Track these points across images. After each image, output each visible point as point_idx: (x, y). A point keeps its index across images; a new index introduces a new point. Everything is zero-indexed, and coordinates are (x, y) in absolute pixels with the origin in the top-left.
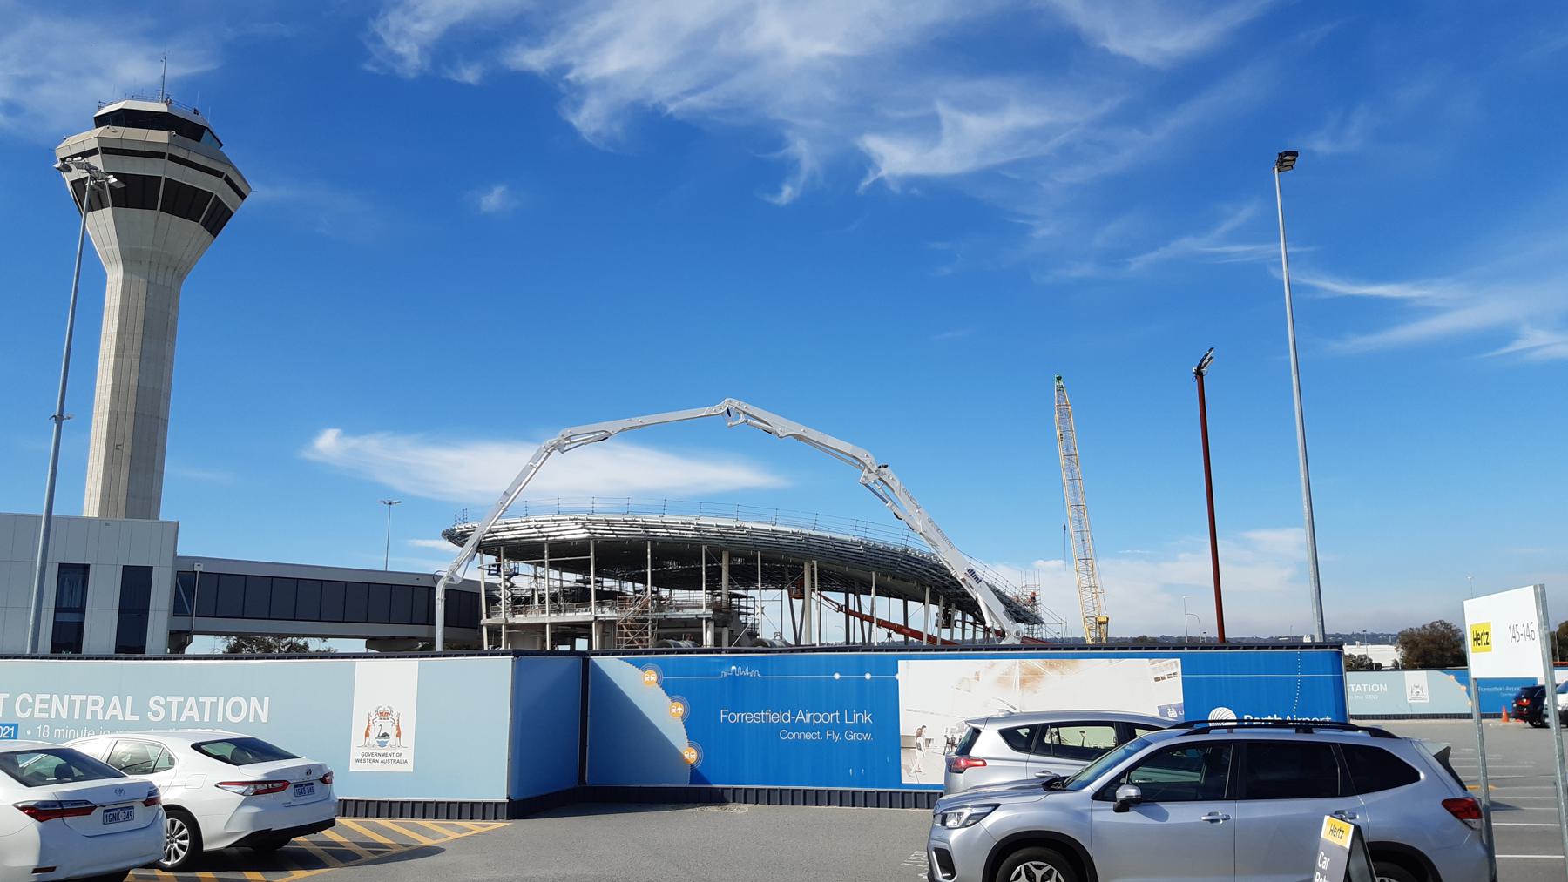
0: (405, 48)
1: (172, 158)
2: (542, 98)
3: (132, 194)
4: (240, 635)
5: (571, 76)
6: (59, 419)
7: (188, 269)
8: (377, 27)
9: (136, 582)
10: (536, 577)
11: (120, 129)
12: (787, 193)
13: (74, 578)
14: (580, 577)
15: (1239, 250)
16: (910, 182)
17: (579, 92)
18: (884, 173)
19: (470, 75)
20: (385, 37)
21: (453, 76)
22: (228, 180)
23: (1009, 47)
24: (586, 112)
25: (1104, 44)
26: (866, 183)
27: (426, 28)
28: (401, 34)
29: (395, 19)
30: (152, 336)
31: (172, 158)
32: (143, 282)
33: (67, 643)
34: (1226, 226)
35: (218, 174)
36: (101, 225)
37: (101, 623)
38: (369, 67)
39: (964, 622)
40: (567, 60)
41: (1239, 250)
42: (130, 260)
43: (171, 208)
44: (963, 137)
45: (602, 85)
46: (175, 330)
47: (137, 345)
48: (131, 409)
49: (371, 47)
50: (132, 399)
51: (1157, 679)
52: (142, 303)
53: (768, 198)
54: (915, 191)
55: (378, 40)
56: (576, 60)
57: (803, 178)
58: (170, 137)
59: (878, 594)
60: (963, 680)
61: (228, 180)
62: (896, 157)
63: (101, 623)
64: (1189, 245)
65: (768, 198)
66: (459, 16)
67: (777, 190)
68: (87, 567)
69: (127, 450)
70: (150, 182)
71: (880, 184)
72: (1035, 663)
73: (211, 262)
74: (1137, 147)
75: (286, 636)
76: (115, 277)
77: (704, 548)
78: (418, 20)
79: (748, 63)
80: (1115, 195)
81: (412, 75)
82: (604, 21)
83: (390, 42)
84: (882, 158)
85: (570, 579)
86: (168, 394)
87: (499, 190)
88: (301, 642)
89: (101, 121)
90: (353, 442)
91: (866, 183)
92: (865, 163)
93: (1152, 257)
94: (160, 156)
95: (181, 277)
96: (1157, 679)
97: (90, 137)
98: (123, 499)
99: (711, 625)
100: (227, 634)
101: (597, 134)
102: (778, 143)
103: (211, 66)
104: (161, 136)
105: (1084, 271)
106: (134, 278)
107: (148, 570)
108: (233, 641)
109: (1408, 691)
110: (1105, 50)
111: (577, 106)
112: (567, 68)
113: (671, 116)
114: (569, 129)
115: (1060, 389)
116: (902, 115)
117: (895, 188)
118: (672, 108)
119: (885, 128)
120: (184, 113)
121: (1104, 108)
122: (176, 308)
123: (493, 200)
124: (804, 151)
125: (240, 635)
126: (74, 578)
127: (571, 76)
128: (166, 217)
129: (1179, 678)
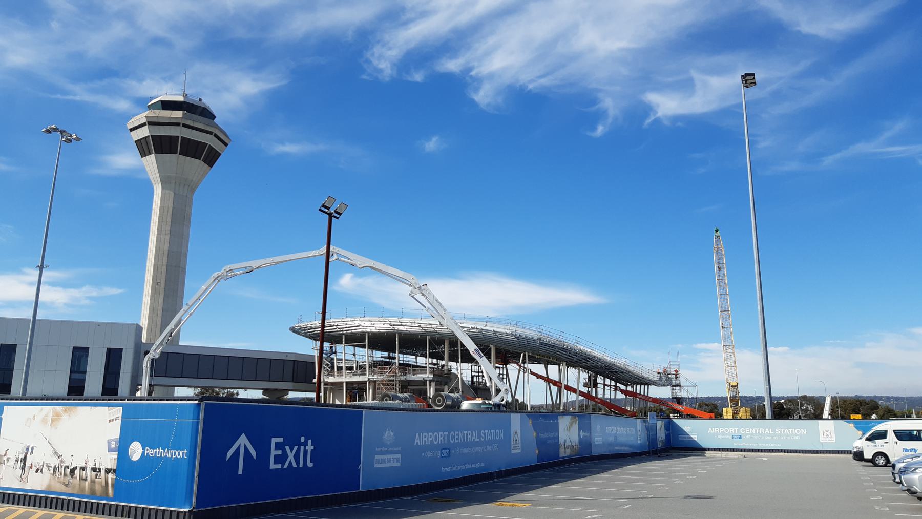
0: (384, 65)
1: (184, 125)
2: (455, 88)
3: (160, 145)
4: (202, 388)
5: (473, 73)
6: (41, 268)
7: (197, 185)
8: (368, 55)
9: (113, 357)
10: (354, 355)
11: (157, 111)
12: (600, 130)
13: (80, 355)
14: (386, 354)
15: (897, 150)
16: (676, 118)
17: (478, 81)
18: (660, 114)
19: (418, 77)
20: (372, 59)
21: (410, 79)
22: (216, 136)
23: (734, 34)
24: (482, 93)
25: (798, 28)
26: (648, 121)
27: (394, 53)
28: (381, 57)
29: (377, 50)
30: (178, 222)
31: (184, 125)
32: (172, 193)
33: (76, 390)
34: (887, 134)
35: (211, 133)
36: (151, 162)
37: (94, 382)
38: (364, 77)
39: (605, 385)
40: (471, 64)
41: (897, 150)
42: (165, 182)
43: (185, 153)
44: (712, 89)
45: (491, 76)
46: (190, 219)
47: (168, 228)
48: (165, 263)
49: (365, 66)
50: (165, 258)
51: (110, 421)
52: (171, 205)
53: (589, 133)
54: (680, 124)
55: (368, 61)
56: (476, 64)
57: (610, 120)
58: (184, 114)
59: (462, 362)
60: (29, 419)
61: (216, 136)
62: (667, 105)
63: (94, 382)
64: (863, 148)
65: (589, 133)
66: (412, 45)
67: (594, 129)
68: (87, 349)
69: (163, 285)
70: (173, 140)
71: (657, 121)
72: (59, 408)
73: (212, 182)
74: (821, 90)
75: (224, 389)
76: (158, 190)
77: (428, 338)
78: (390, 49)
79: (575, 57)
80: (814, 118)
81: (387, 79)
82: (491, 41)
83: (375, 62)
84: (658, 105)
85: (378, 355)
86: (186, 255)
87: (435, 139)
88: (235, 391)
89: (150, 107)
90: (359, 280)
91: (648, 121)
92: (648, 109)
93: (838, 156)
94: (178, 124)
95: (193, 191)
96: (110, 421)
97: (141, 118)
98: (160, 312)
99: (433, 384)
100: (196, 387)
101: (488, 105)
102: (594, 101)
103: (284, 82)
104: (178, 114)
105: (793, 166)
106: (167, 191)
107: (120, 351)
108: (199, 390)
109: (821, 436)
110: (799, 32)
111: (477, 90)
112: (470, 69)
113: (530, 91)
114: (473, 103)
115: (717, 237)
116: (670, 80)
117: (666, 123)
118: (531, 86)
119: (660, 88)
120: (194, 100)
121: (803, 65)
122: (191, 207)
123: (432, 145)
124: (610, 105)
125: (202, 388)
126: (80, 355)
127: (473, 73)
128: (183, 157)
129: (119, 421)
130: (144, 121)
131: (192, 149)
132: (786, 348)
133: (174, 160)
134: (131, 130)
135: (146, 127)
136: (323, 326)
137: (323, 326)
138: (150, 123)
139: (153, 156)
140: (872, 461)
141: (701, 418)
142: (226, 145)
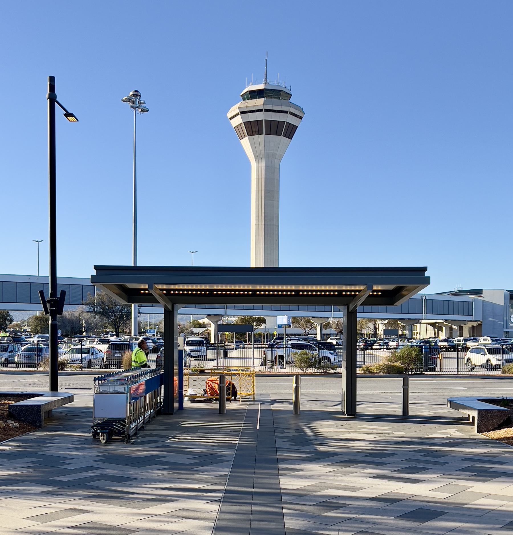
1: (266, 110)
22: (292, 114)
31: (266, 110)
35: (286, 112)
43: (269, 132)
61: (292, 114)
104: (259, 102)
130: (238, 111)
131: (274, 128)
132: (162, 330)
133: (261, 138)
134: (230, 119)
135: (239, 116)
136: (406, 385)
137: (406, 385)
138: (242, 113)
139: (247, 138)
140: (71, 115)
141: (448, 293)
142: (301, 118)
